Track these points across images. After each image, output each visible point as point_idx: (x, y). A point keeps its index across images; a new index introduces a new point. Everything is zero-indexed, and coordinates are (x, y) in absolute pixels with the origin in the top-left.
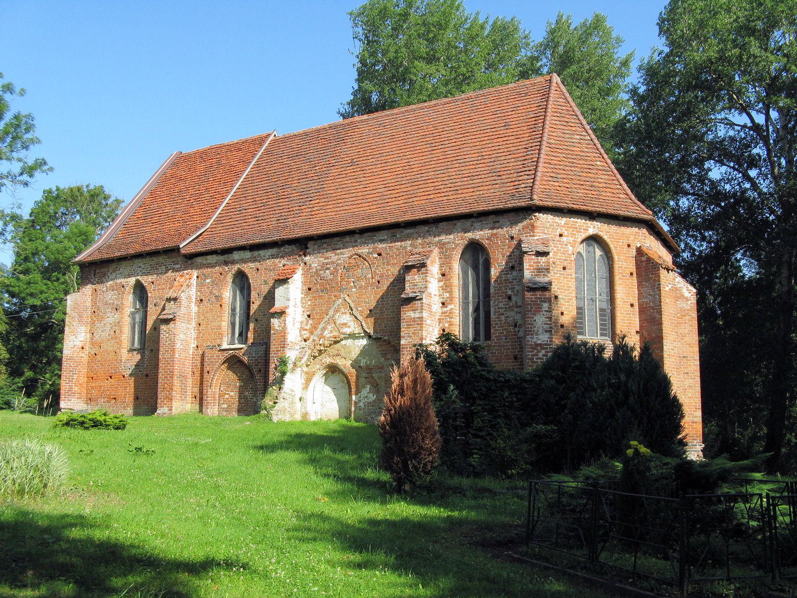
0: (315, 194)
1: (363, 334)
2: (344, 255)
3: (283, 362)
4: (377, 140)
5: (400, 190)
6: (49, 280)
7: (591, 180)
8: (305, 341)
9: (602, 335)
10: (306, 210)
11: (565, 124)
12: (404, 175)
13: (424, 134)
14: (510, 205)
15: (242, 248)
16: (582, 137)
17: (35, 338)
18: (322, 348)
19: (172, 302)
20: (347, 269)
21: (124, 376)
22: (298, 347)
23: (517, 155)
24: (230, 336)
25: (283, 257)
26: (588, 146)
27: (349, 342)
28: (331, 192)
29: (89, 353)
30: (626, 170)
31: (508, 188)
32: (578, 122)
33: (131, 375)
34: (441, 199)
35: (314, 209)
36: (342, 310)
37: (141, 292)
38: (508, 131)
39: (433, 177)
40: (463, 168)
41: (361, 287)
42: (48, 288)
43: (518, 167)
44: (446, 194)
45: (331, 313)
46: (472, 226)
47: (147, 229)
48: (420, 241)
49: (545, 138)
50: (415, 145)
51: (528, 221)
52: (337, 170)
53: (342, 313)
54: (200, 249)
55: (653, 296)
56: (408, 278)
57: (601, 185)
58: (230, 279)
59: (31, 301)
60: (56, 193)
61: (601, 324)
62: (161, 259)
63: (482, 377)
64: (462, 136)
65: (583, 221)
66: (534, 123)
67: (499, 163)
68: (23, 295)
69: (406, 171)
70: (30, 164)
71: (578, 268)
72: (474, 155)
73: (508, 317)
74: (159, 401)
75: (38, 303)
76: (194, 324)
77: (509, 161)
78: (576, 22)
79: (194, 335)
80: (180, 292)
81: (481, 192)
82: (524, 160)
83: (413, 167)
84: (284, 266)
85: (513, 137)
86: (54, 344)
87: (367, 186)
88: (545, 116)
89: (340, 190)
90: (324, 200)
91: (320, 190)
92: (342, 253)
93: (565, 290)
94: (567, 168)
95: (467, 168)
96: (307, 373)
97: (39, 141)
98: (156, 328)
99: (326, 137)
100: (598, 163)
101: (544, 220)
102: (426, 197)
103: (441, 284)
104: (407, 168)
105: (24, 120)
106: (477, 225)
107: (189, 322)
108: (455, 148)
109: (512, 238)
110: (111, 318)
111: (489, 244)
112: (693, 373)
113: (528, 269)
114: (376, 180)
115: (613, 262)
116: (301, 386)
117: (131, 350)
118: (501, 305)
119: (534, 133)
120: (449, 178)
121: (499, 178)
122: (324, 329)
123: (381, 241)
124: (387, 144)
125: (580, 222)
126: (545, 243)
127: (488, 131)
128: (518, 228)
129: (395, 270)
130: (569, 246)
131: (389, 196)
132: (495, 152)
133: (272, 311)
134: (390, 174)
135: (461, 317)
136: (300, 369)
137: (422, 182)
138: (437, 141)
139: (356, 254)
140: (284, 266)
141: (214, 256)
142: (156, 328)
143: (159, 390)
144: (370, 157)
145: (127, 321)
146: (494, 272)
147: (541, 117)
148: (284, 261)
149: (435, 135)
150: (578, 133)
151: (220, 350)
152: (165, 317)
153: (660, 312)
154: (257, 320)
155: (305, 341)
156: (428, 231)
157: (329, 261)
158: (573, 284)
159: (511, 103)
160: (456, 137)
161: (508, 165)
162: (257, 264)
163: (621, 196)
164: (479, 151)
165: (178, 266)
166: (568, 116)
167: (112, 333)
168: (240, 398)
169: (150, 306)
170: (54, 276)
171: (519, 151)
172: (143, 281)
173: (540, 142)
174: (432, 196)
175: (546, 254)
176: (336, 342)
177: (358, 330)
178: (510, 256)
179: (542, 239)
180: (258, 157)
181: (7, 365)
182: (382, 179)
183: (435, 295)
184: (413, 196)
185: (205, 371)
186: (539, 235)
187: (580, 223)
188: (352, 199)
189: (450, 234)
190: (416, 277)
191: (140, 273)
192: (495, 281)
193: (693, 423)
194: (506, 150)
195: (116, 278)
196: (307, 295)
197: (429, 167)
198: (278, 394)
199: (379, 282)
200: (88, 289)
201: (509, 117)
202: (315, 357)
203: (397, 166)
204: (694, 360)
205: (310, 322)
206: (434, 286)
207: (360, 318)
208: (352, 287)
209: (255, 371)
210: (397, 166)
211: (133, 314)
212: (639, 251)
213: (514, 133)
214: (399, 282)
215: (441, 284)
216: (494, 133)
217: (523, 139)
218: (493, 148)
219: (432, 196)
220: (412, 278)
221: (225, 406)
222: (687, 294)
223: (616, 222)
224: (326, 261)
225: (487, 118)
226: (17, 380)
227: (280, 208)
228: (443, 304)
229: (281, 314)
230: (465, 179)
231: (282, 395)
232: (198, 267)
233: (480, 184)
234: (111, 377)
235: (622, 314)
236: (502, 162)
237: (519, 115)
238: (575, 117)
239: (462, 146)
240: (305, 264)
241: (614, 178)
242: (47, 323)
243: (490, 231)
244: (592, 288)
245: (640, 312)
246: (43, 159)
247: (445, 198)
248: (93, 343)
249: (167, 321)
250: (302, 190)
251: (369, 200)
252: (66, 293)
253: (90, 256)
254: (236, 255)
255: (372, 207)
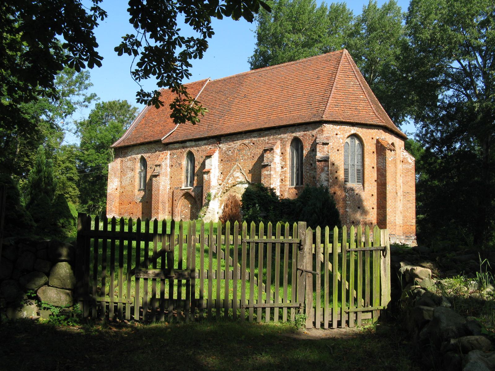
0: (226, 113)
1: (246, 182)
2: (237, 144)
3: (209, 195)
4: (258, 84)
5: (265, 111)
6: (99, 153)
7: (356, 106)
8: (220, 185)
9: (357, 182)
10: (221, 121)
11: (346, 76)
12: (268, 103)
13: (280, 81)
14: (312, 120)
15: (191, 140)
16: (354, 83)
17: (93, 183)
18: (228, 188)
19: (158, 167)
20: (239, 150)
21: (136, 203)
22: (216, 188)
23: (321, 94)
24: (186, 183)
25: (209, 145)
26: (357, 88)
27: (240, 186)
28: (234, 112)
29: (120, 191)
30: (382, 97)
31: (314, 111)
32: (354, 75)
33: (140, 202)
34: (283, 116)
35: (225, 120)
36: (237, 170)
37: (143, 161)
38: (318, 80)
39: (281, 105)
40: (295, 100)
41: (245, 159)
42: (99, 157)
43: (320, 100)
44: (286, 114)
45: (232, 171)
46: (295, 130)
47: (147, 130)
48: (272, 137)
49: (334, 85)
50: (275, 87)
51: (320, 127)
52: (238, 100)
53: (237, 172)
54: (171, 141)
55: (383, 163)
56: (265, 155)
57: (360, 108)
58: (185, 155)
59: (89, 165)
60: (102, 105)
61: (357, 177)
62: (153, 146)
63: (273, 201)
64: (297, 83)
65: (349, 127)
66: (331, 76)
67: (312, 97)
68: (86, 161)
69: (269, 101)
70: (88, 97)
71: (346, 151)
72: (301, 93)
73: (310, 174)
74: (152, 214)
75: (94, 165)
76: (169, 177)
77: (316, 97)
78: (379, 6)
79: (169, 183)
80: (162, 162)
81: (301, 113)
82: (323, 96)
83: (272, 99)
84: (210, 149)
85: (320, 84)
86: (103, 186)
87: (251, 109)
88: (337, 73)
89: (238, 111)
90: (230, 116)
91: (229, 111)
92: (236, 143)
93: (338, 161)
94: (344, 100)
95: (297, 100)
96: (221, 201)
97: (93, 85)
98: (151, 180)
99: (234, 82)
100: (362, 97)
101: (327, 127)
102: (276, 115)
103: (281, 158)
104: (270, 99)
105: (85, 74)
106: (297, 129)
107: (166, 176)
108: (293, 89)
109: (313, 136)
110: (130, 174)
111: (303, 139)
112: (412, 201)
113: (319, 151)
114: (255, 106)
115: (364, 146)
116: (218, 207)
117: (139, 190)
118: (308, 168)
119: (330, 82)
120: (288, 105)
121: (311, 106)
122: (228, 179)
123: (254, 137)
124: (262, 87)
125: (347, 128)
126: (328, 138)
127: (309, 80)
128: (316, 131)
129: (260, 151)
130: (341, 139)
131: (260, 114)
132: (311, 92)
133: (204, 171)
134: (262, 103)
135: (291, 174)
136: (217, 198)
137: (276, 107)
138: (285, 85)
139: (243, 143)
140: (210, 149)
141: (178, 144)
142: (151, 180)
143: (152, 209)
144: (254, 93)
145: (137, 176)
146: (305, 152)
147: (335, 73)
148: (210, 147)
149: (285, 82)
150: (353, 81)
151: (181, 190)
152: (155, 174)
153: (386, 171)
154: (198, 175)
155: (220, 185)
156: (275, 133)
157: (231, 146)
158: (342, 158)
159: (322, 65)
160: (294, 83)
161: (316, 99)
162: (198, 148)
163: (371, 113)
164: (304, 91)
165: (161, 149)
166: (349, 72)
167: (130, 182)
168: (191, 213)
169: (148, 168)
170: (102, 151)
171: (322, 91)
172: (144, 157)
173: (332, 87)
174: (279, 115)
175: (327, 144)
176: (234, 186)
177: (243, 180)
178: (312, 144)
179: (327, 136)
180: (201, 92)
181: (79, 197)
182: (258, 105)
183: (278, 163)
184: (271, 114)
185: (174, 200)
186: (325, 134)
187: (347, 128)
188: (243, 116)
189: (286, 134)
190: (269, 155)
191: (143, 153)
192: (306, 157)
193: (411, 225)
194: (316, 91)
195: (132, 155)
196: (221, 163)
197: (280, 99)
198: (207, 210)
199: (253, 157)
200: (119, 160)
201: (320, 73)
202: (224, 193)
203: (265, 98)
204: (413, 194)
205: (222, 176)
206: (277, 158)
207: (244, 174)
208: (241, 159)
209: (197, 199)
210: (265, 98)
211: (140, 173)
212: (378, 141)
213: (321, 82)
214: (261, 158)
215: (281, 158)
216: (312, 82)
217: (324, 85)
218: (310, 90)
219: (279, 115)
220: (267, 155)
221: (184, 216)
222: (410, 161)
223: (367, 127)
224: (230, 147)
225: (310, 73)
226: (84, 206)
227: (210, 120)
228: (282, 167)
229: (208, 172)
230: (295, 106)
231: (208, 211)
232: (170, 150)
233: (301, 109)
234: (130, 203)
235: (368, 172)
236: (313, 97)
237: (325, 72)
238: (352, 72)
239: (296, 88)
240: (220, 148)
241: (369, 104)
242: (99, 175)
243: (303, 133)
244: (353, 159)
245: (377, 171)
246: (95, 94)
247: (285, 116)
248: (121, 187)
249: (156, 176)
250: (220, 110)
251: (251, 116)
252: (108, 160)
253: (119, 144)
254: (188, 144)
255: (252, 120)
